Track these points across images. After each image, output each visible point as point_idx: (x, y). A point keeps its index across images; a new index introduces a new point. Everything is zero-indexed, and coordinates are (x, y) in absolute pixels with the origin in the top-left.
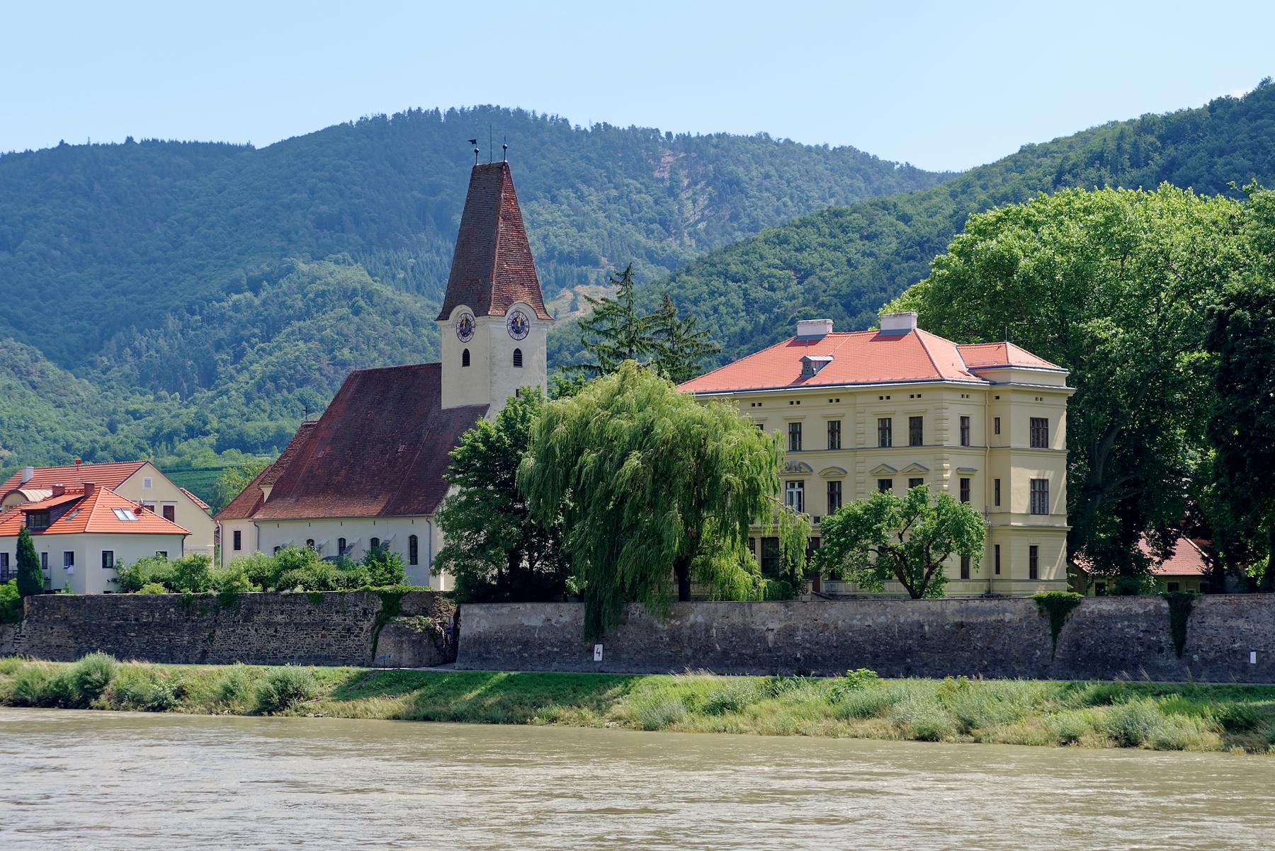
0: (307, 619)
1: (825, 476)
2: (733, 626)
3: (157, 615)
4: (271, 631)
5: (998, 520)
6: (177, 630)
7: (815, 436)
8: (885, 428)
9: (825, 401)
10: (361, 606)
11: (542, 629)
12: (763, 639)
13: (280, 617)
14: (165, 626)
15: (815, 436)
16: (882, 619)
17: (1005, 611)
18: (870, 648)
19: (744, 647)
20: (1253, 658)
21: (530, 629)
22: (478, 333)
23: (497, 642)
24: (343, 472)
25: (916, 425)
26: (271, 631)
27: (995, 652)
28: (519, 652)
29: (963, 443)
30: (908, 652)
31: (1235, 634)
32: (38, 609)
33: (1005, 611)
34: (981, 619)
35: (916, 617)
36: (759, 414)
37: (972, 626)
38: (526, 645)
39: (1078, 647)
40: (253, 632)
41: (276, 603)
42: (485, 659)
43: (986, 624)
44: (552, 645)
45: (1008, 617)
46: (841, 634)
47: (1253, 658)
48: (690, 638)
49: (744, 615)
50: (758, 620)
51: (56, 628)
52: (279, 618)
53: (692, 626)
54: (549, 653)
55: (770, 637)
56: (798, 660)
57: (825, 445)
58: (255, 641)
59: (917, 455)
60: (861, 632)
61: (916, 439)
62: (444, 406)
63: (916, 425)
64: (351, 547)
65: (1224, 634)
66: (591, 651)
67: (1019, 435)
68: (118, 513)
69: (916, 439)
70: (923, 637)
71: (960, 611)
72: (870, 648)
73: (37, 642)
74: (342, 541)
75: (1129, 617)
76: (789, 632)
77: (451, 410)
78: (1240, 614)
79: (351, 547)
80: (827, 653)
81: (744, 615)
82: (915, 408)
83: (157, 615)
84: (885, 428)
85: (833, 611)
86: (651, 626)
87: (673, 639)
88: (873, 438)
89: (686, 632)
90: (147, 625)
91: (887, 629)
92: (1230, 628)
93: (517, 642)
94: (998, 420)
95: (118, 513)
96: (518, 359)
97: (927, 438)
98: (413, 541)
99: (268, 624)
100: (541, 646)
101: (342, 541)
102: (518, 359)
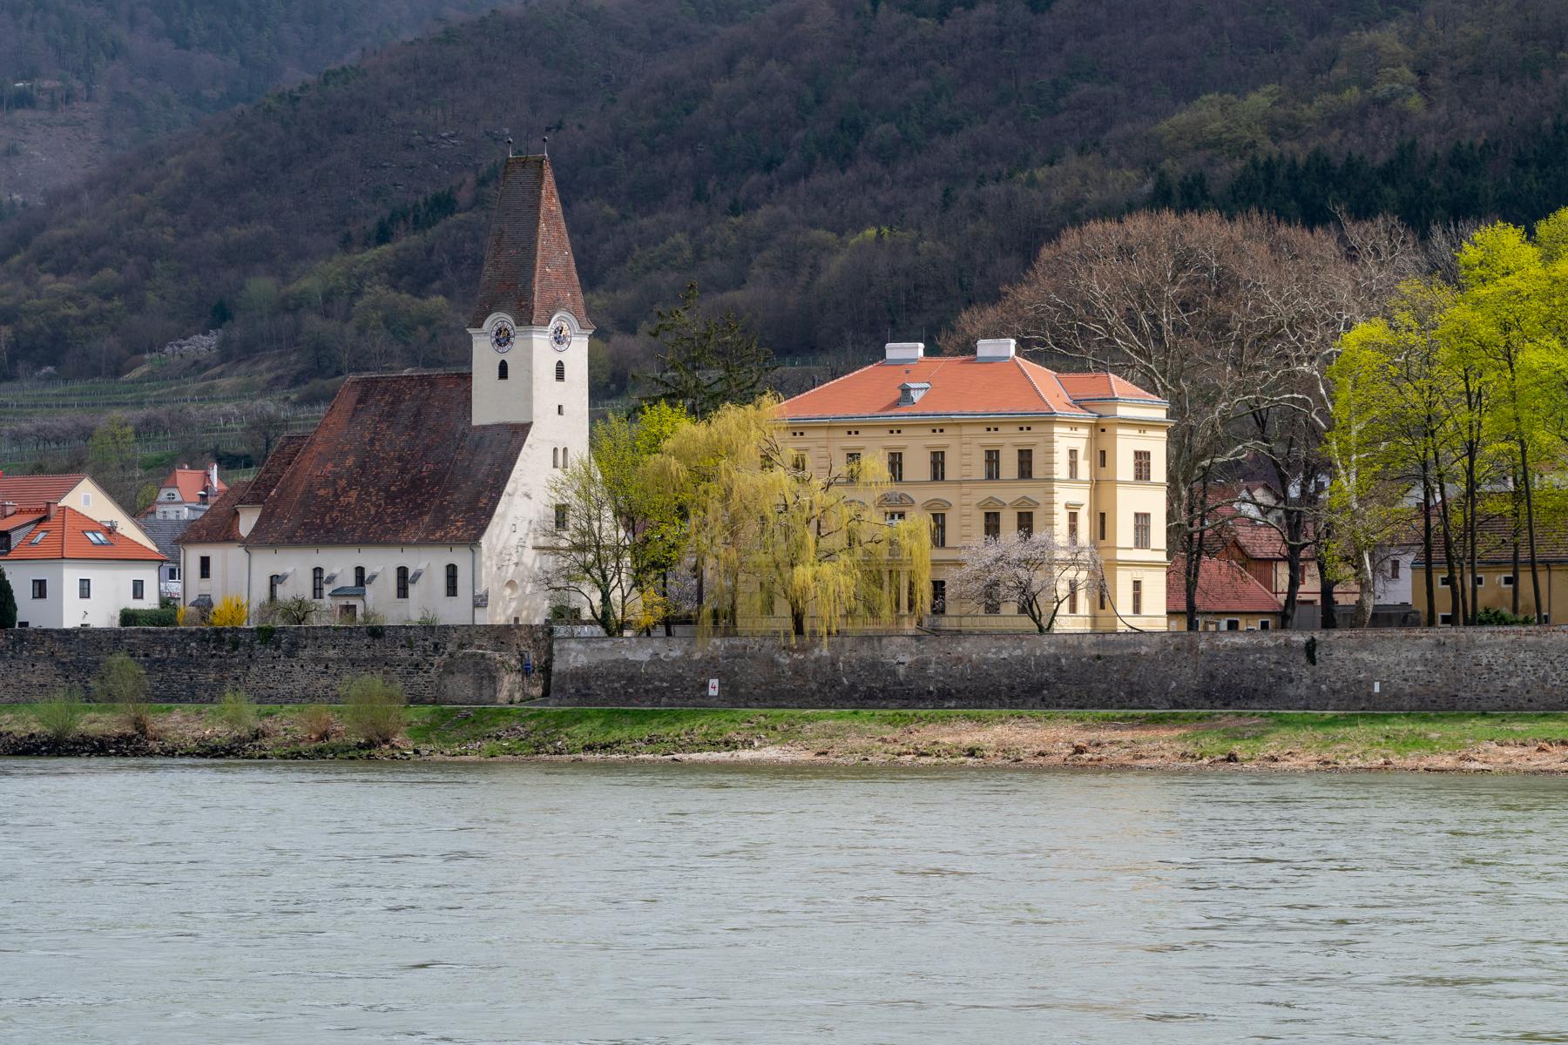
0: (366, 654)
1: (927, 508)
2: (861, 660)
3: (173, 650)
4: (321, 668)
5: (1106, 554)
6: (199, 666)
7: (917, 466)
8: (992, 458)
9: (983, 430)
10: (431, 640)
11: (651, 662)
12: (894, 673)
13: (331, 652)
14: (187, 661)
15: (917, 466)
16: (1018, 652)
17: (1141, 644)
18: (1005, 681)
19: (874, 680)
20: (1377, 689)
21: (635, 664)
22: (518, 343)
23: (597, 677)
24: (354, 494)
25: (1025, 458)
26: (321, 668)
27: (1132, 684)
28: (623, 687)
29: (935, 477)
30: (1045, 684)
31: (1360, 665)
32: (14, 644)
33: (1141, 644)
34: (1118, 652)
35: (1052, 650)
36: (853, 443)
37: (1110, 659)
38: (631, 680)
39: (1213, 677)
40: (297, 668)
41: (326, 637)
42: (586, 695)
43: (1121, 657)
44: (662, 680)
45: (1144, 650)
46: (976, 667)
47: (1377, 689)
48: (815, 673)
49: (873, 649)
50: (888, 653)
51: (39, 665)
52: (331, 653)
53: (817, 660)
54: (657, 689)
55: (901, 670)
56: (930, 693)
57: (927, 476)
58: (301, 679)
59: (938, 492)
60: (996, 664)
61: (1025, 471)
62: (474, 423)
63: (1025, 458)
64: (373, 577)
65: (1350, 665)
66: (705, 686)
67: (1125, 467)
68: (90, 535)
69: (1025, 471)
70: (1060, 669)
71: (1096, 644)
72: (1005, 681)
73: (13, 681)
74: (360, 571)
75: (1260, 649)
76: (922, 665)
77: (484, 427)
78: (1364, 646)
79: (373, 577)
80: (962, 686)
81: (873, 649)
82: (1025, 440)
83: (173, 650)
84: (992, 458)
85: (967, 645)
86: (772, 661)
87: (796, 672)
88: (979, 470)
89: (811, 666)
90: (162, 662)
91: (1023, 661)
92: (1356, 660)
93: (620, 677)
94: (1103, 453)
95: (90, 535)
96: (560, 374)
97: (1037, 472)
98: (452, 571)
99: (316, 660)
100: (648, 681)
101: (360, 571)
102: (560, 374)
